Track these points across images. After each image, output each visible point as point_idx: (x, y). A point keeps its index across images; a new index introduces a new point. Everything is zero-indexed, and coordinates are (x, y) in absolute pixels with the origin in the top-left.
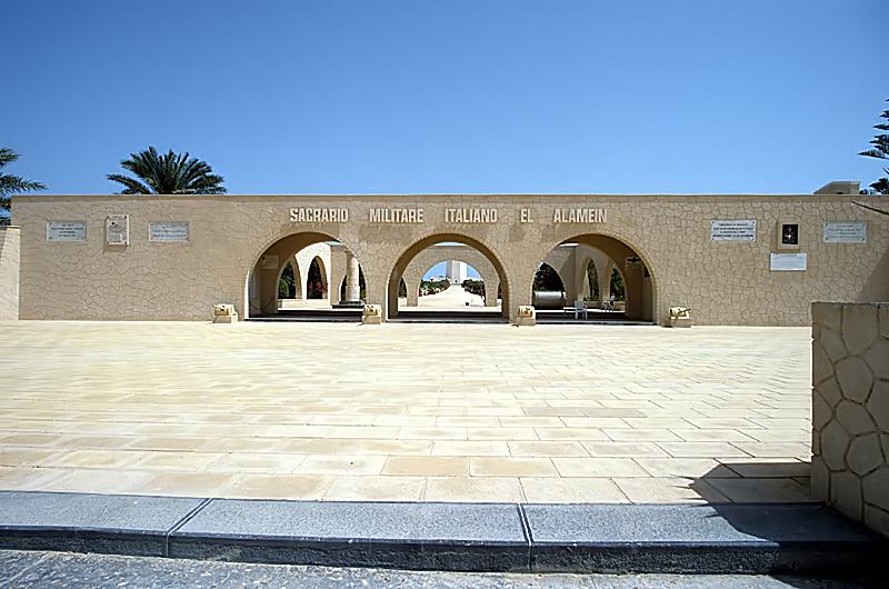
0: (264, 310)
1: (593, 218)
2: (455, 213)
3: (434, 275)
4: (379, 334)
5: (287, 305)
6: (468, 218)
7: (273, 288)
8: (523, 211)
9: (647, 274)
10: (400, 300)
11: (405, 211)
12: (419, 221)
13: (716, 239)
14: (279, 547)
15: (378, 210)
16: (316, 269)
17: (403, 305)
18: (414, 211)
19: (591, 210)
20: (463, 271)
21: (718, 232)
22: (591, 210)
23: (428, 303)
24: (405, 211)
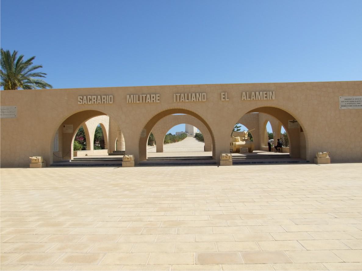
0: (59, 160)
1: (266, 97)
2: (180, 96)
3: (174, 130)
4: (130, 174)
5: (81, 154)
6: (188, 99)
7: (63, 148)
8: (222, 94)
9: (302, 130)
10: (148, 147)
11: (148, 96)
12: (157, 101)
13: (343, 108)
14: (243, 202)
15: (132, 96)
16: (100, 130)
17: (151, 152)
18: (154, 95)
19: (264, 93)
20: (196, 130)
21: (344, 104)
22: (264, 93)
23: (171, 150)
24: (148, 96)
